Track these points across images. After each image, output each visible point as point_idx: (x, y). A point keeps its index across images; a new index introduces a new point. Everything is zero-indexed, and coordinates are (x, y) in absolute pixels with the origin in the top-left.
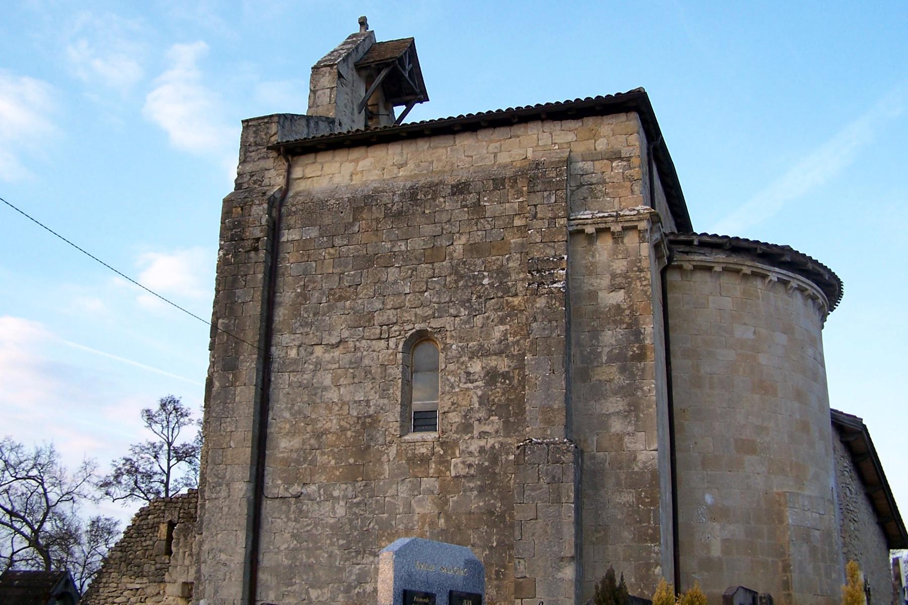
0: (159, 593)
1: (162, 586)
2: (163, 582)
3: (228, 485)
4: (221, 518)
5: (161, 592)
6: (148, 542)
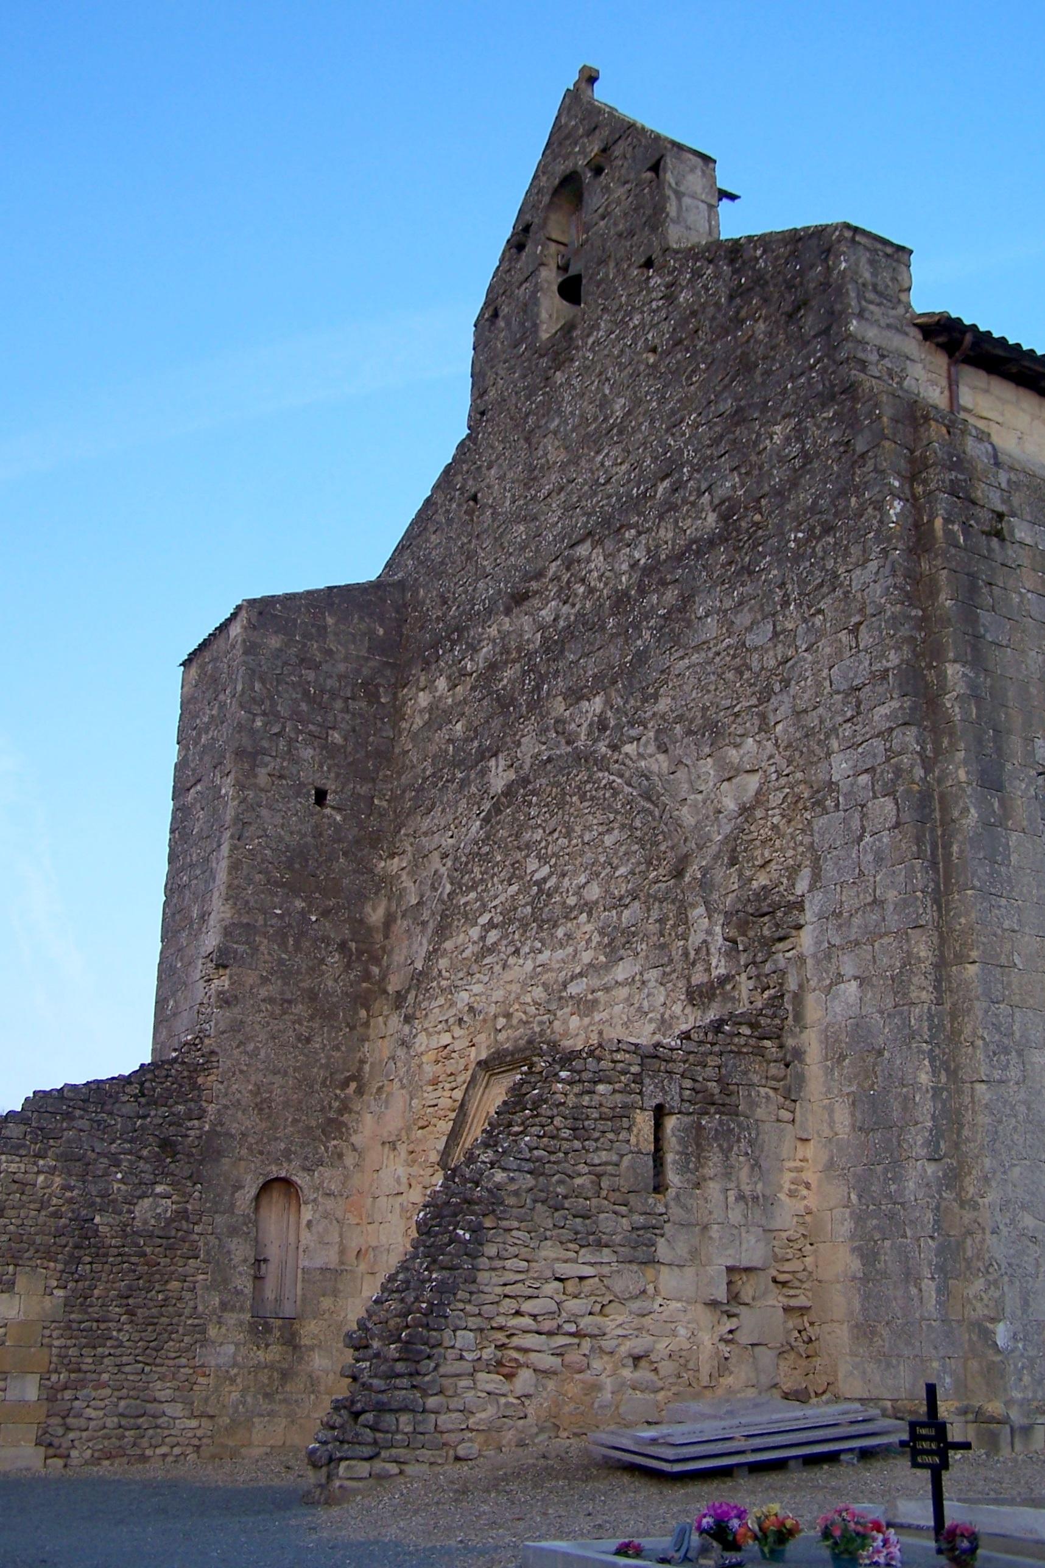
0: (644, 1292)
1: (650, 1272)
2: (652, 1261)
3: (1020, 1054)
4: (1015, 1128)
5: (650, 1289)
6: (604, 1156)
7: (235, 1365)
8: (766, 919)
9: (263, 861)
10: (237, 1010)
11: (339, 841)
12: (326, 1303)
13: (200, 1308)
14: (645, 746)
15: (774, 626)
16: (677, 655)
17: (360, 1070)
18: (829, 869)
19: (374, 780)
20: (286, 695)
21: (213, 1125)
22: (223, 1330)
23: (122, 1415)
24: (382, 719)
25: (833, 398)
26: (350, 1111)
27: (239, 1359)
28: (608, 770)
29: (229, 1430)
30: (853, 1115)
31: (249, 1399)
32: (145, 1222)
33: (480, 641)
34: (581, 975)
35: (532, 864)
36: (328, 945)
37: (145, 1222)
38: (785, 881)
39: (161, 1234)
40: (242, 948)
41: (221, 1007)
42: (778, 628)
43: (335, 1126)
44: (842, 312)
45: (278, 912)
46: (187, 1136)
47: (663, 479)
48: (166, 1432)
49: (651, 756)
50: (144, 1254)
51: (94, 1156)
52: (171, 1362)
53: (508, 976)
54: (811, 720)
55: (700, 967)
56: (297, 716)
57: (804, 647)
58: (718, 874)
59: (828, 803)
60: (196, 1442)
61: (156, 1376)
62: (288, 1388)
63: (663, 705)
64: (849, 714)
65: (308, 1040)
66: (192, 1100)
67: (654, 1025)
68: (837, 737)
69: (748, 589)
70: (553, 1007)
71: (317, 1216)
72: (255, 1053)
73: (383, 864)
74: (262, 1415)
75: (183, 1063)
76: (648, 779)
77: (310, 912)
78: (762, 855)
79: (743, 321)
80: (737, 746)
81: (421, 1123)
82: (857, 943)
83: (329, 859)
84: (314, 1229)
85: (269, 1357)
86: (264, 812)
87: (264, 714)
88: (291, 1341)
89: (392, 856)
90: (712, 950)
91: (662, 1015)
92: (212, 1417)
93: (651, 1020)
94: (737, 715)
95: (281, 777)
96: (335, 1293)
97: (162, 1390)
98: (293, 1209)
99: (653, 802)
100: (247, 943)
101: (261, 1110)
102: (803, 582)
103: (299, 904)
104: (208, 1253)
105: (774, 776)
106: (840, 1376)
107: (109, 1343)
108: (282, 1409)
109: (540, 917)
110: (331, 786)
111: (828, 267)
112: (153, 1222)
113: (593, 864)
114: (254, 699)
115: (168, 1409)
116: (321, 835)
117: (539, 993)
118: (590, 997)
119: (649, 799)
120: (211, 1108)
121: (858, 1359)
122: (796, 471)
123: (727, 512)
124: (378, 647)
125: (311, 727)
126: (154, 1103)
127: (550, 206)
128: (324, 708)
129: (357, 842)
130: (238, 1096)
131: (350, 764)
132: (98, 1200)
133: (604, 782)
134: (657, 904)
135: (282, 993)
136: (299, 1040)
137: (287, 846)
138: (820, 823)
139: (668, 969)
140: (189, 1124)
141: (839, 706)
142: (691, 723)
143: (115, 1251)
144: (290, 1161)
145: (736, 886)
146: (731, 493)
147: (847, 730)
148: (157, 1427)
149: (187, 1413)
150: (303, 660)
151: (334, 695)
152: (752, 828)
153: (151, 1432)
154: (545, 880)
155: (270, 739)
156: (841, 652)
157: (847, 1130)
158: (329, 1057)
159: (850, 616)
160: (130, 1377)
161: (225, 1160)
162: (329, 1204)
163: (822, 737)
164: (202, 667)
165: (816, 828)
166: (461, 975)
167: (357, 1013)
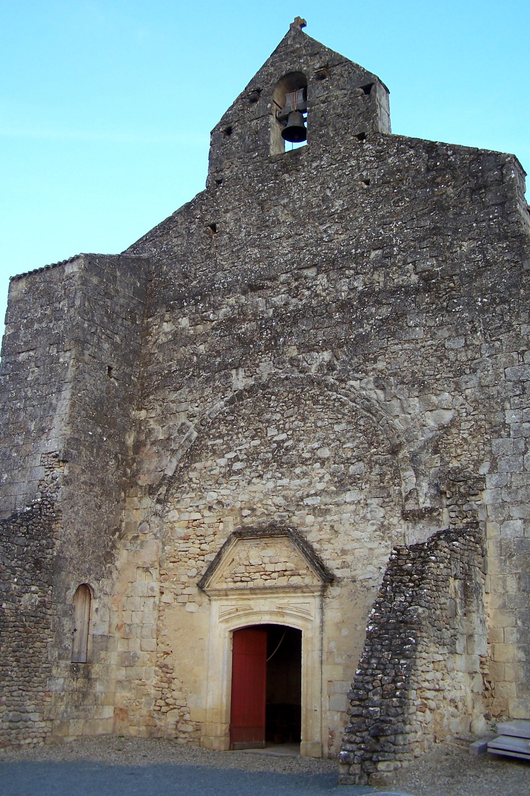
7: (63, 690)
8: (461, 483)
9: (85, 403)
10: (71, 487)
11: (117, 397)
12: (103, 654)
13: (49, 658)
14: (367, 384)
15: (466, 341)
16: (392, 342)
17: (121, 525)
18: (502, 464)
19: (132, 366)
20: (98, 312)
21: (58, 552)
22: (59, 670)
23: (11, 721)
24: (137, 333)
25: (506, 238)
26: (116, 548)
27: (65, 686)
28: (336, 391)
29: (60, 727)
30: (519, 583)
31: (69, 710)
32: (26, 608)
33: (220, 305)
34: (316, 494)
35: (272, 431)
36: (110, 455)
37: (26, 608)
38: (472, 466)
39: (33, 615)
40: (74, 452)
41: (64, 485)
42: (468, 343)
43: (109, 557)
44: (512, 198)
45: (91, 433)
46: (46, 558)
47: (374, 250)
48: (31, 730)
49: (371, 389)
50: (24, 626)
51: (4, 568)
52: (34, 689)
53: (251, 488)
54: (493, 391)
55: (411, 501)
56: (102, 325)
57: (487, 355)
58: (425, 457)
59: (503, 433)
60: (44, 735)
61: (28, 697)
62: (85, 703)
63: (381, 365)
64: (518, 393)
65: (100, 507)
66: (49, 537)
67: (375, 527)
68: (510, 402)
69: (446, 319)
70: (292, 509)
71: (101, 606)
72: (77, 513)
73: (134, 413)
74: (73, 718)
75: (46, 516)
76: (369, 401)
77: (103, 435)
78: (456, 452)
79: (438, 184)
80: (436, 395)
81: (173, 559)
82: (522, 502)
83: (112, 407)
84: (99, 613)
85: (78, 685)
86: (87, 376)
87: (89, 320)
88: (87, 676)
89: (140, 409)
90: (421, 494)
91: (382, 523)
92: (52, 720)
93: (373, 524)
94: (438, 380)
95: (94, 357)
96: (106, 649)
97: (30, 706)
98: (87, 602)
99: (372, 413)
100: (76, 449)
101: (79, 545)
102: (486, 323)
103: (99, 430)
104: (54, 626)
105: (465, 414)
106: (510, 707)
107: (7, 678)
108: (82, 714)
109: (281, 459)
110: (115, 366)
111: (502, 173)
112: (29, 608)
113: (325, 439)
114: (85, 310)
115: (31, 716)
116: (109, 392)
117: (279, 500)
118: (323, 507)
119: (369, 411)
120: (58, 543)
121: (523, 700)
122: (479, 268)
123: (427, 278)
124: (138, 293)
125: (108, 332)
126: (32, 538)
127: (276, 85)
128: (114, 322)
129: (124, 399)
130: (70, 536)
131: (123, 355)
132: (5, 594)
133: (334, 397)
134: (377, 466)
135: (90, 480)
136: (96, 506)
137: (95, 397)
138: (495, 442)
139: (387, 500)
140: (47, 551)
141: (510, 388)
142: (404, 378)
143: (12, 624)
144: (90, 575)
145: (439, 464)
146: (431, 268)
147: (517, 400)
148: (27, 727)
149: (41, 719)
150: (106, 293)
151: (118, 317)
152: (449, 437)
153: (23, 730)
154: (283, 441)
155: (91, 334)
156: (513, 363)
157: (515, 590)
158: (108, 517)
159: (520, 346)
160: (16, 699)
161: (63, 573)
162: (106, 599)
163: (499, 401)
164: (33, 284)
165: (493, 443)
166: (210, 483)
167: (120, 494)
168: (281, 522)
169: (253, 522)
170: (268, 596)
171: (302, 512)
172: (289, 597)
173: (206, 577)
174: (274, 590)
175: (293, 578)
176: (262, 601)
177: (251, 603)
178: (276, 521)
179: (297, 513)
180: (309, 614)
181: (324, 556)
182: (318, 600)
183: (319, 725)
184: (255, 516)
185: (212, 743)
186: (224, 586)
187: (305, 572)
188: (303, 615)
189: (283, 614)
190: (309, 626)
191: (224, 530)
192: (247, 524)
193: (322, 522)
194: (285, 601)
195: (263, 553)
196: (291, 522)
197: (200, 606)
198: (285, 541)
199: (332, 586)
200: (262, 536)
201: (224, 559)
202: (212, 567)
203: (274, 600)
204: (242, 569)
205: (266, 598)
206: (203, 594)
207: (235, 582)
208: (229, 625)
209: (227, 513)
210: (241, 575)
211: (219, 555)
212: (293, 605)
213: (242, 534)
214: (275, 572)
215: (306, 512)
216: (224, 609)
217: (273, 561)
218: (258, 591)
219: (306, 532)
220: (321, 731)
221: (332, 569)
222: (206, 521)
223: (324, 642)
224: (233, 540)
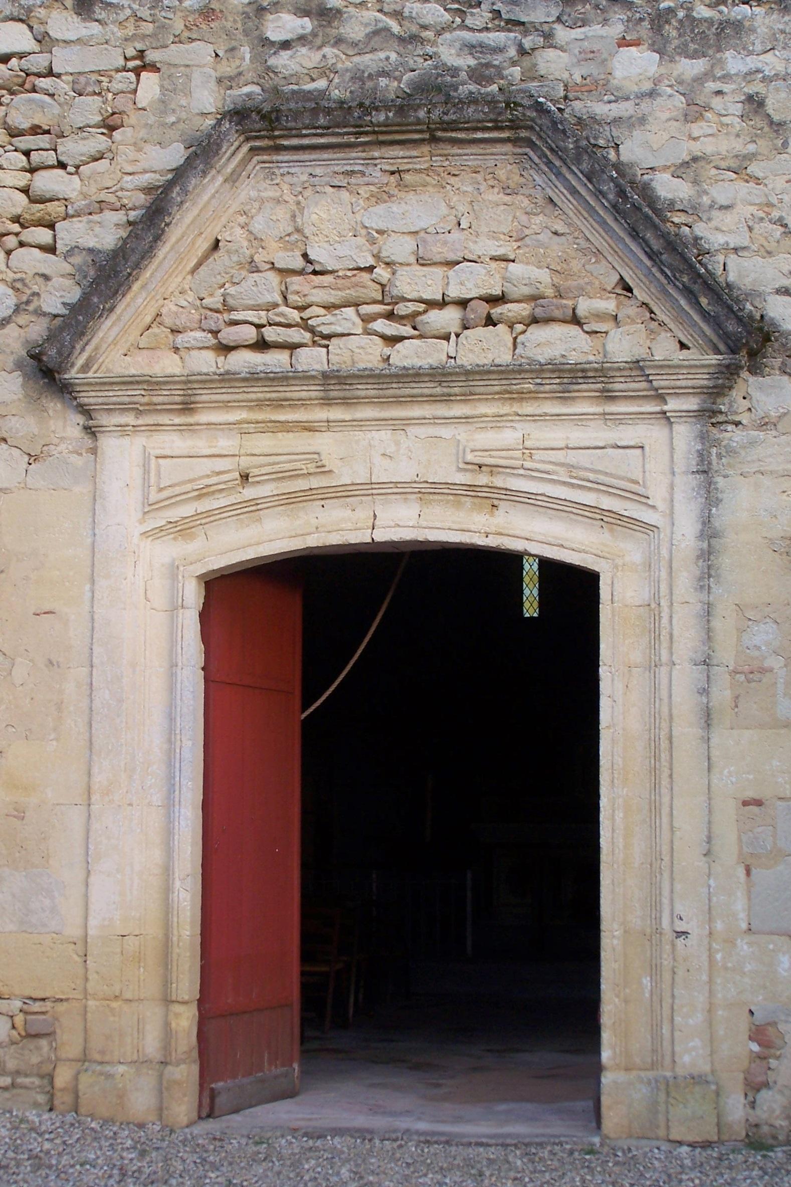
168: (478, 75)
169: (325, 71)
170: (416, 411)
171: (596, 29)
172: (533, 418)
173: (79, 319)
174: (449, 383)
175: (537, 334)
176: (385, 435)
177: (325, 444)
178: (454, 71)
179: (562, 34)
180: (642, 498)
181: (716, 233)
182: (685, 435)
183: (701, 999)
184: (339, 41)
185: (121, 1096)
186: (168, 365)
187: (609, 305)
188: (606, 503)
189: (491, 498)
190: (632, 550)
191: (163, 105)
192: (295, 77)
193: (700, 80)
194: (509, 436)
195: (376, 217)
196: (531, 75)
197: (33, 458)
198: (502, 162)
199: (755, 370)
200: (383, 137)
201: (173, 235)
202: (108, 278)
203: (446, 432)
204: (268, 287)
205: (408, 421)
206: (54, 406)
207: (225, 349)
208: (191, 548)
209: (178, 26)
210: (261, 317)
211: (154, 216)
212: (559, 456)
213: (269, 124)
214: (442, 304)
215: (616, 29)
216: (170, 472)
217: (437, 251)
218: (362, 390)
219: (618, 121)
220: (710, 1023)
221: (752, 295)
222: (62, 60)
223: (716, 624)
224: (227, 150)
